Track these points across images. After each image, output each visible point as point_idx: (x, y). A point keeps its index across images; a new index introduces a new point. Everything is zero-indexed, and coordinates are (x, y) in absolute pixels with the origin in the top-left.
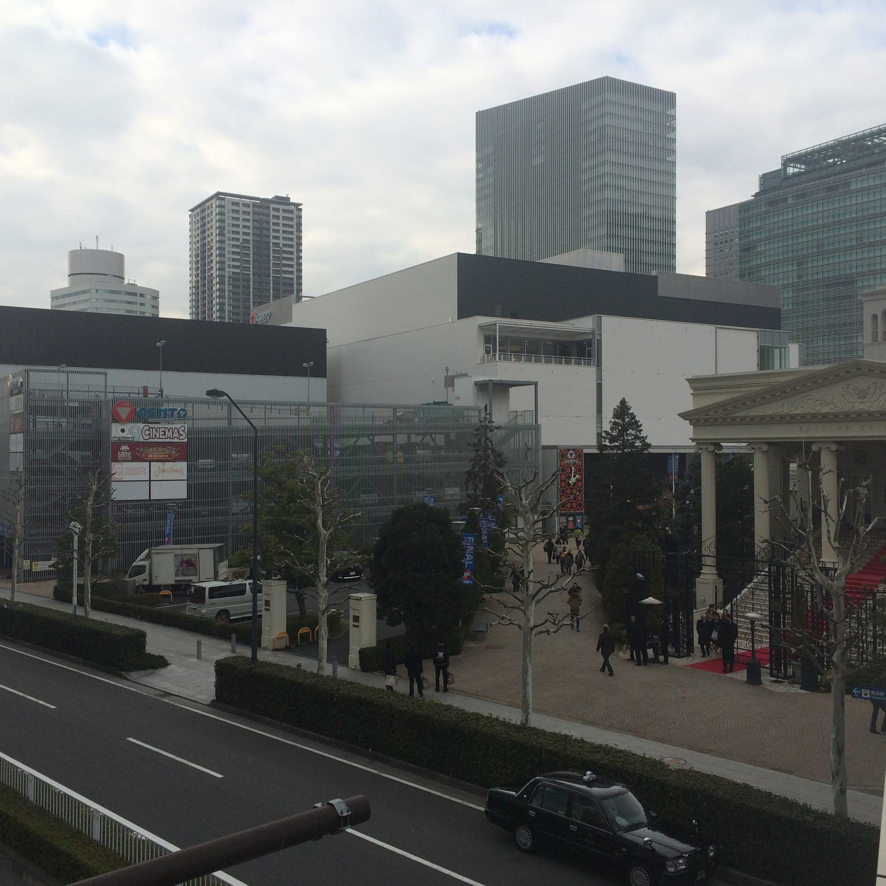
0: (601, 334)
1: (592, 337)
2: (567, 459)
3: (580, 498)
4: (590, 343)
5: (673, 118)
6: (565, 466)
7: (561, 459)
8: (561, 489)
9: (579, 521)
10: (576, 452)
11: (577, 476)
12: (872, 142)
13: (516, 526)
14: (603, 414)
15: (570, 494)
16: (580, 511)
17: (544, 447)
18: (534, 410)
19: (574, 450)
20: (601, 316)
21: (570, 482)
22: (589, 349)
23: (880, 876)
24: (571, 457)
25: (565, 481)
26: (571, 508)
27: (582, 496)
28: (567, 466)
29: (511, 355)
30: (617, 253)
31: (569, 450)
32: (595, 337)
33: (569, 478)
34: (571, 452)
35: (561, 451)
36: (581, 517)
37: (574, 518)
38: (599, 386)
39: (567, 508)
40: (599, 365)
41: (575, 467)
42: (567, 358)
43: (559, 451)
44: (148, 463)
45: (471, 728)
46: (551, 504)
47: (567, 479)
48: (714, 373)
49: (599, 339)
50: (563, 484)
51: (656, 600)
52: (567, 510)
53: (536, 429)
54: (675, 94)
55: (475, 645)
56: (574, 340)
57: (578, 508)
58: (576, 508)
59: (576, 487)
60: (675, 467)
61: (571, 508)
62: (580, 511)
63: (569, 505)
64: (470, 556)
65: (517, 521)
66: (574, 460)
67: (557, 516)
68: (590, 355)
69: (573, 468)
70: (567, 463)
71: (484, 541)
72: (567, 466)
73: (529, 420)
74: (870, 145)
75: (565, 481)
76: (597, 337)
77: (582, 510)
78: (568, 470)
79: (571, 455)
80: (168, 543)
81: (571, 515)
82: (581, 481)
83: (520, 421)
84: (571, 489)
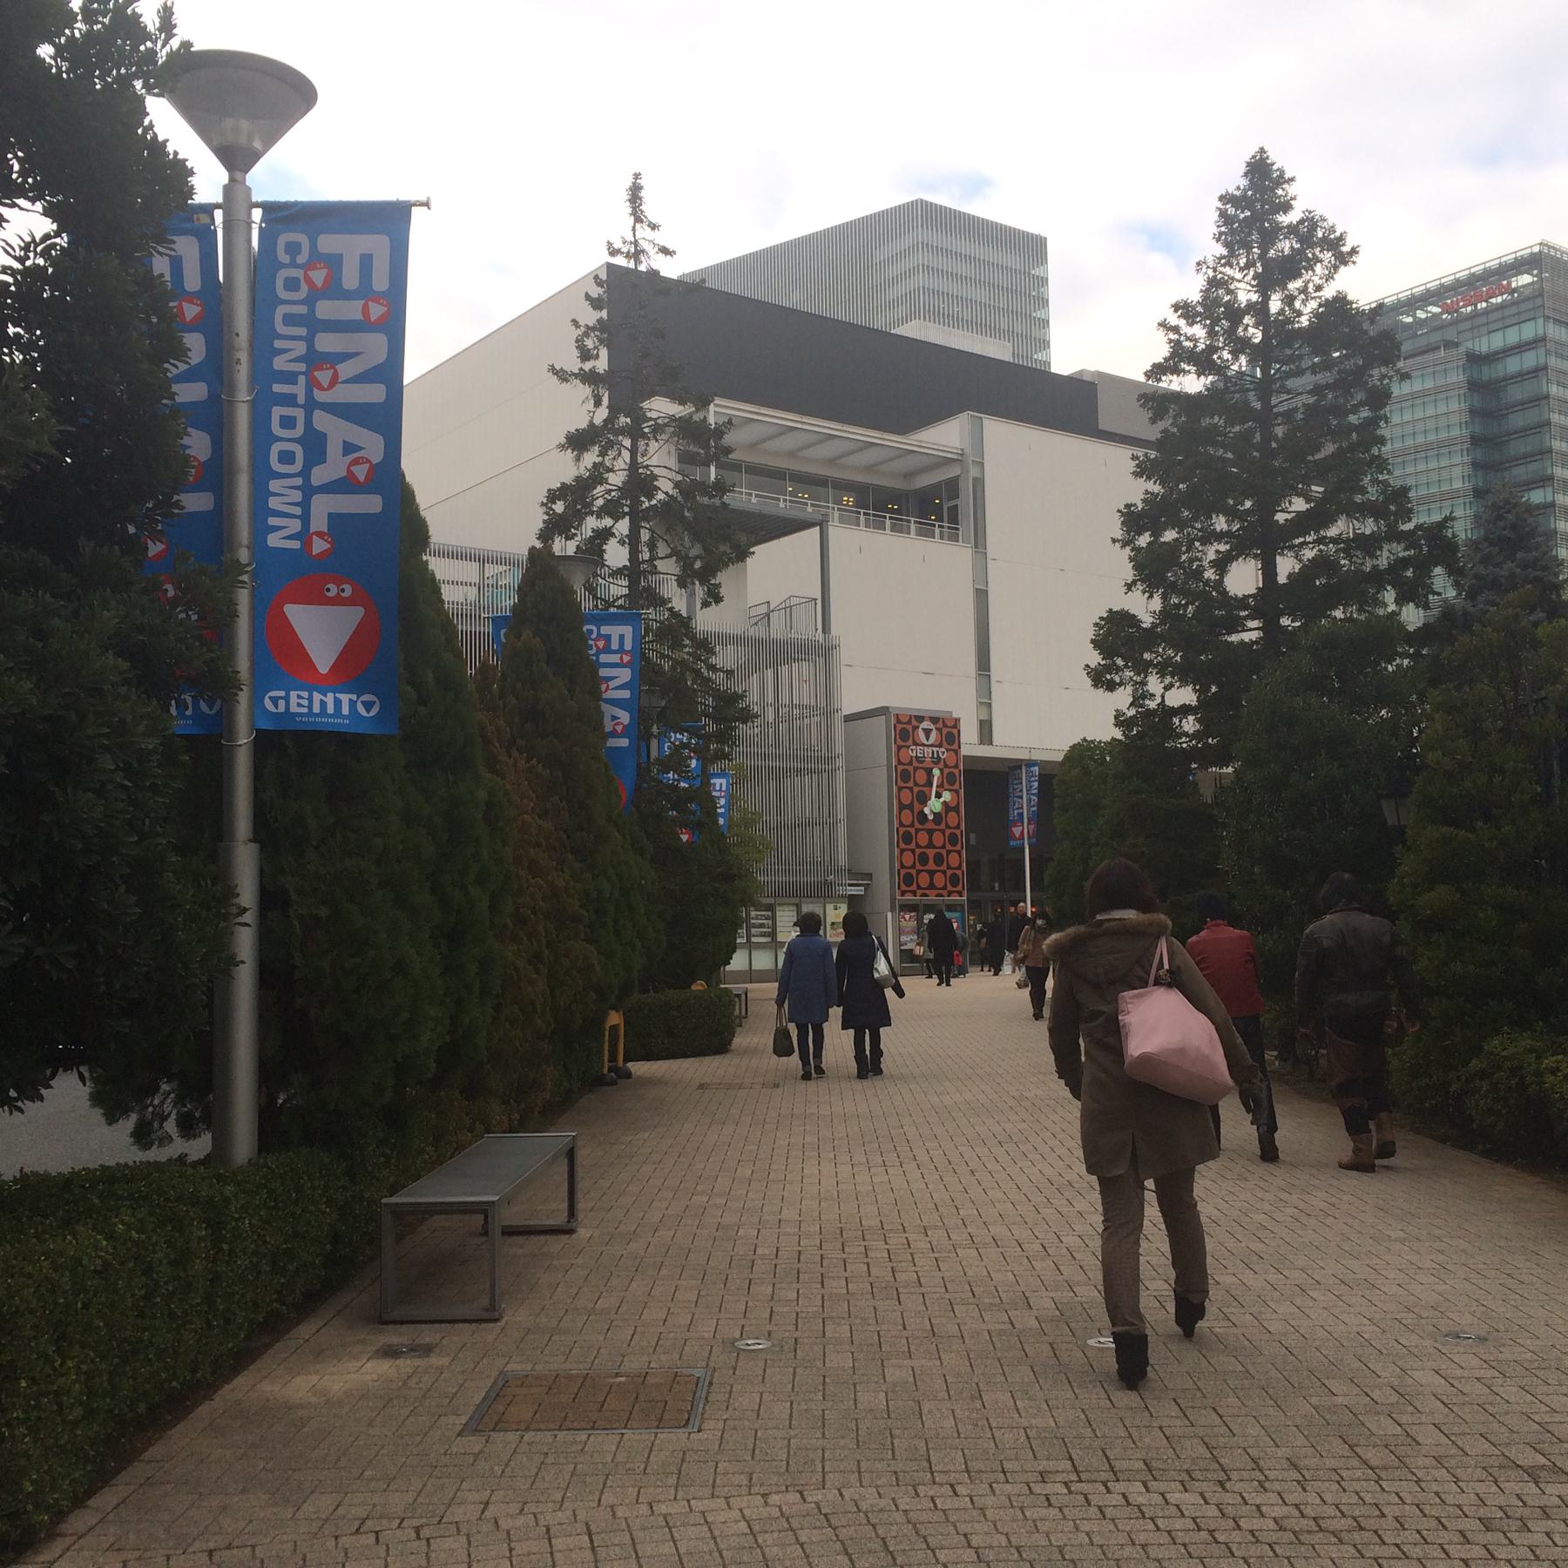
0: (982, 464)
1: (959, 473)
2: (916, 744)
3: (953, 859)
4: (952, 488)
5: (1044, 281)
6: (911, 763)
7: (900, 742)
8: (902, 830)
10: (940, 725)
11: (947, 796)
12: (1414, 316)
14: (992, 669)
15: (926, 847)
17: (849, 718)
18: (819, 596)
19: (934, 720)
20: (981, 418)
21: (926, 810)
22: (953, 503)
23: (1399, 822)
24: (928, 740)
25: (910, 807)
26: (932, 886)
28: (915, 764)
29: (751, 495)
30: (998, 340)
31: (920, 719)
32: (968, 471)
33: (924, 799)
34: (926, 725)
35: (899, 721)
38: (982, 596)
39: (919, 887)
40: (979, 542)
41: (941, 770)
43: (893, 721)
46: (871, 880)
47: (916, 803)
49: (978, 475)
50: (907, 817)
52: (919, 892)
53: (822, 653)
54: (1046, 239)
55: (385, 1367)
56: (912, 488)
57: (950, 888)
58: (944, 888)
59: (943, 826)
61: (932, 886)
63: (924, 880)
66: (935, 749)
67: (892, 910)
68: (954, 518)
69: (936, 772)
70: (916, 757)
72: (915, 764)
73: (806, 628)
74: (1409, 323)
75: (910, 807)
76: (974, 472)
78: (921, 777)
79: (927, 732)
82: (956, 809)
83: (778, 629)
84: (930, 832)
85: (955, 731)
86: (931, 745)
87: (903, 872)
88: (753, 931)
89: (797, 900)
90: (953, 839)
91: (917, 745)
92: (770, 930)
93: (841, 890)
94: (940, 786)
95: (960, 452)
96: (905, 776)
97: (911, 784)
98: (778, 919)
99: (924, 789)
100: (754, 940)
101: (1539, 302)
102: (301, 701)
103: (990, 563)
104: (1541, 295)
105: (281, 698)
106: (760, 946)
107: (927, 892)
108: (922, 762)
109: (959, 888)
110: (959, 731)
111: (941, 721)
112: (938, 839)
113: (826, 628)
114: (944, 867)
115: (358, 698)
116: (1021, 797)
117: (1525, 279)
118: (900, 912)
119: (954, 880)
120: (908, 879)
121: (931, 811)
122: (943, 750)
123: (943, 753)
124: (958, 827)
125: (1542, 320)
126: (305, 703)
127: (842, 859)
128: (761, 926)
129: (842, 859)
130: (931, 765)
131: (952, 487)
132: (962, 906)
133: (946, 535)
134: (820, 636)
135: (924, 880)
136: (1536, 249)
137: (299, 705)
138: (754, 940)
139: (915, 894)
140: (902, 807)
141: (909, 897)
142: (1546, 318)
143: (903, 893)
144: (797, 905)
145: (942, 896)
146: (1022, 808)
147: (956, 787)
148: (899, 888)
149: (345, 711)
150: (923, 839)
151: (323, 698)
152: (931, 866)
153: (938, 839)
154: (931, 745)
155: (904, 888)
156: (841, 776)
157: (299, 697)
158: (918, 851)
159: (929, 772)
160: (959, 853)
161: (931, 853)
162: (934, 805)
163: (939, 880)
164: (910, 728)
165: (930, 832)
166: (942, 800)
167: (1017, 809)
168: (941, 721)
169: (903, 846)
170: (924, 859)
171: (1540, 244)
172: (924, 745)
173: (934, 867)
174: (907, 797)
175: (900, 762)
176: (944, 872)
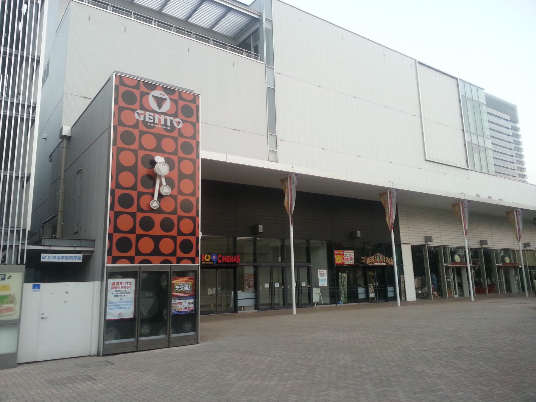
2: (142, 108)
10: (176, 96)
19: (169, 90)
23: (359, 293)
24: (160, 107)
27: (194, 220)
28: (142, 128)
31: (151, 86)
34: (157, 93)
40: (270, 63)
44: (393, 291)
48: (359, 292)
51: (239, 43)
52: (139, 258)
57: (180, 254)
58: (173, 254)
61: (156, 252)
66: (169, 118)
76: (266, 25)
77: (193, 260)
79: (160, 101)
80: (470, 265)
91: (145, 110)
102: (150, 117)
109: (192, 254)
111: (177, 93)
115: (174, 119)
122: (178, 120)
123: (178, 123)
126: (152, 118)
132: (196, 272)
135: (146, 245)
137: (150, 119)
139: (131, 260)
143: (115, 260)
145: (170, 262)
149: (169, 124)
151: (160, 117)
154: (165, 114)
155: (116, 253)
157: (150, 115)
164: (137, 93)
168: (177, 93)
169: (118, 208)
170: (147, 224)
173: (160, 232)
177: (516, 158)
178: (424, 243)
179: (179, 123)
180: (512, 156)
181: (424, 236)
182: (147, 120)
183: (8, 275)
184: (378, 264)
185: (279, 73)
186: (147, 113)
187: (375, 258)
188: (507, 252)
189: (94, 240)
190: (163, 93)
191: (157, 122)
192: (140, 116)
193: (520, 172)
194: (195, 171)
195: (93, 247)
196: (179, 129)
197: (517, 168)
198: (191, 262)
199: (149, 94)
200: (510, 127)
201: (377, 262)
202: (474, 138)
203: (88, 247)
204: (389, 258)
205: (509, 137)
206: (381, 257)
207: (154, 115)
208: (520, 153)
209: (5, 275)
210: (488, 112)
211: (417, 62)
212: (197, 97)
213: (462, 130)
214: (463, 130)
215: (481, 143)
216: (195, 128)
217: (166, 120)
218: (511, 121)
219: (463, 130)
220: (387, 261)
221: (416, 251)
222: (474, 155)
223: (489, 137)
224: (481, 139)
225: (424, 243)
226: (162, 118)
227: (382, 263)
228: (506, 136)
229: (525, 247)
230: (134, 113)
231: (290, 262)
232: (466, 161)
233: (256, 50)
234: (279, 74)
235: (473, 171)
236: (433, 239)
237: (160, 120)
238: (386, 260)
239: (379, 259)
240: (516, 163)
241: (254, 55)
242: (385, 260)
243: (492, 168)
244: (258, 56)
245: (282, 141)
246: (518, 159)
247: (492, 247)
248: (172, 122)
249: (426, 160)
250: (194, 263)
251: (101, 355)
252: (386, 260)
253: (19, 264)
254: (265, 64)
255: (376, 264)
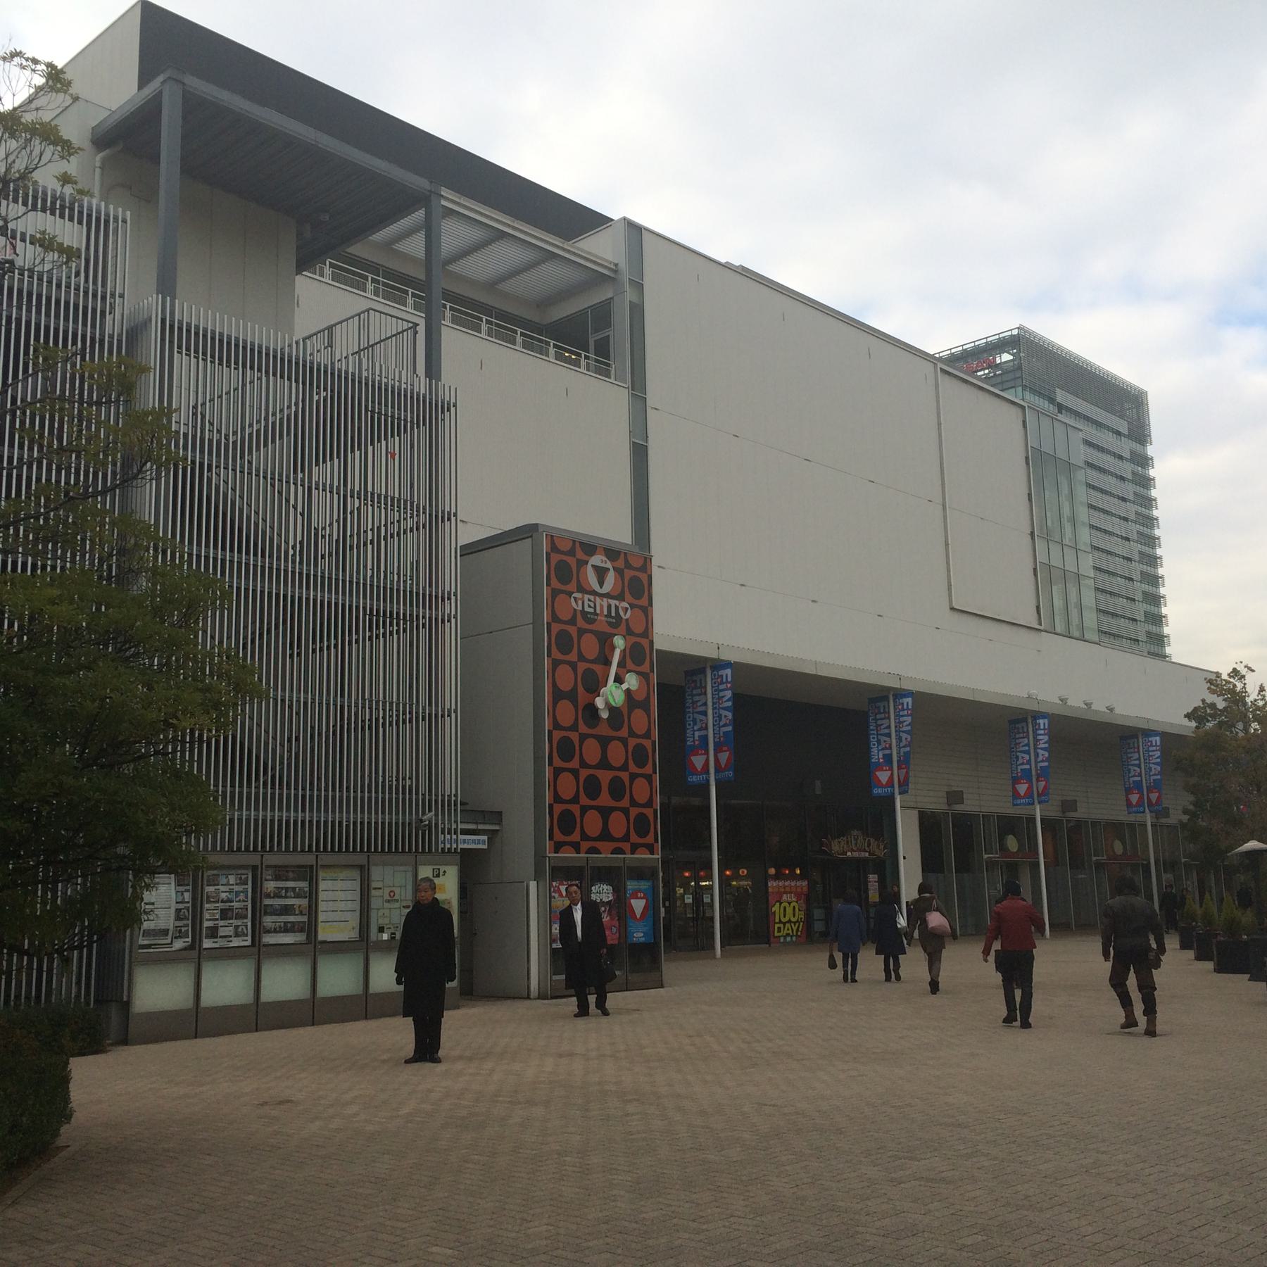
1: (610, 295)
3: (640, 790)
6: (573, 621)
8: (558, 735)
9: (638, 905)
13: (310, 928)
15: (597, 767)
16: (643, 855)
17: (469, 550)
21: (599, 702)
24: (601, 584)
26: (606, 835)
33: (595, 686)
34: (597, 560)
35: (554, 548)
36: (644, 885)
37: (616, 891)
38: (640, 454)
39: (585, 837)
42: (532, 338)
45: (420, 887)
46: (500, 823)
47: (581, 689)
49: (635, 299)
50: (566, 712)
52: (585, 845)
57: (634, 838)
58: (626, 838)
60: (899, 739)
61: (606, 835)
62: (643, 855)
63: (593, 823)
64: (1156, 766)
65: (313, 896)
66: (613, 602)
67: (538, 876)
69: (619, 642)
70: (583, 612)
71: (587, 989)
72: (581, 622)
75: (572, 696)
76: (630, 295)
78: (590, 646)
81: (606, 874)
82: (645, 705)
84: (604, 742)
85: (644, 577)
86: (607, 596)
87: (558, 808)
88: (268, 921)
89: (361, 859)
90: (640, 756)
92: (305, 919)
93: (447, 841)
94: (621, 664)
95: (612, 266)
96: (564, 642)
97: (573, 657)
98: (322, 896)
99: (595, 667)
100: (269, 939)
101: (1018, 374)
103: (651, 414)
104: (1020, 368)
105: (580, 599)
106: (283, 952)
107: (598, 845)
108: (592, 622)
109: (649, 839)
110: (650, 577)
111: (622, 555)
112: (617, 754)
113: (433, 370)
114: (625, 802)
116: (705, 713)
117: (1006, 357)
118: (552, 879)
119: (642, 825)
120: (566, 823)
121: (607, 704)
122: (625, 604)
124: (648, 735)
125: (1021, 388)
127: (450, 784)
128: (287, 910)
129: (450, 784)
130: (608, 630)
131: (602, 315)
133: (592, 367)
134: (421, 385)
135: (593, 823)
136: (1015, 332)
137: (589, 606)
138: (269, 939)
139: (576, 847)
140: (558, 695)
141: (568, 854)
142: (1024, 387)
143: (558, 847)
144: (361, 868)
146: (706, 728)
147: (645, 668)
148: (551, 838)
150: (592, 751)
152: (605, 799)
153: (617, 754)
154: (607, 596)
155: (559, 836)
156: (451, 636)
158: (584, 773)
159: (605, 643)
160: (649, 778)
161: (605, 777)
162: (612, 694)
163: (618, 824)
164: (572, 561)
165: (604, 742)
166: (625, 686)
167: (699, 730)
168: (622, 555)
169: (558, 762)
170: (592, 787)
171: (1018, 328)
172: (594, 593)
174: (566, 679)
175: (555, 618)
176: (625, 811)
177: (1138, 526)
178: (945, 807)
179: (627, 609)
180: (1128, 539)
181: (946, 789)
182: (587, 609)
183: (442, 868)
184: (856, 854)
185: (656, 409)
186: (587, 597)
187: (848, 842)
188: (1116, 829)
189: (500, 813)
190: (604, 558)
191: (598, 611)
192: (580, 602)
193: (1147, 588)
194: (648, 693)
195: (497, 824)
196: (627, 620)
197: (1141, 594)
198: (648, 852)
199: (587, 562)
200: (1127, 454)
201: (852, 850)
202: (1055, 550)
203: (468, 823)
204: (876, 842)
205: (1119, 463)
206: (861, 838)
207: (595, 599)
208: (1149, 530)
209: (439, 869)
210: (1088, 504)
211: (939, 369)
212: (648, 560)
213: (1029, 533)
214: (1032, 534)
215: (1071, 567)
216: (647, 616)
217: (609, 606)
218: (1129, 437)
219: (1032, 534)
220: (871, 847)
221: (929, 826)
222: (1053, 587)
223: (1089, 549)
224: (1070, 555)
225: (945, 807)
226: (605, 602)
227: (863, 853)
228: (1112, 480)
229: (1157, 818)
230: (570, 597)
231: (710, 848)
232: (1035, 609)
233: (603, 350)
234: (655, 411)
235: (1051, 633)
236: (964, 797)
237: (602, 607)
238: (869, 845)
239: (856, 844)
240: (1137, 542)
241: (597, 361)
242: (868, 846)
243: (1091, 619)
244: (609, 365)
245: (660, 569)
246: (1140, 509)
247: (1086, 816)
248: (617, 607)
249: (952, 609)
250: (652, 853)
251: (549, 997)
252: (869, 845)
253: (218, 852)
254: (628, 388)
255: (849, 854)
